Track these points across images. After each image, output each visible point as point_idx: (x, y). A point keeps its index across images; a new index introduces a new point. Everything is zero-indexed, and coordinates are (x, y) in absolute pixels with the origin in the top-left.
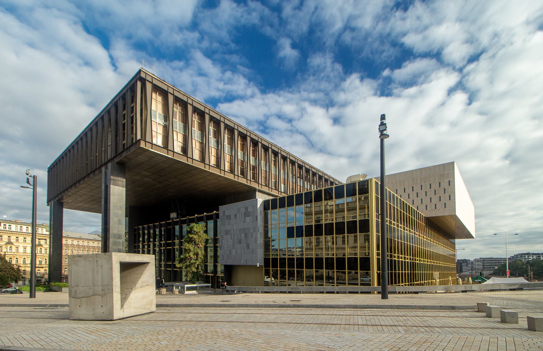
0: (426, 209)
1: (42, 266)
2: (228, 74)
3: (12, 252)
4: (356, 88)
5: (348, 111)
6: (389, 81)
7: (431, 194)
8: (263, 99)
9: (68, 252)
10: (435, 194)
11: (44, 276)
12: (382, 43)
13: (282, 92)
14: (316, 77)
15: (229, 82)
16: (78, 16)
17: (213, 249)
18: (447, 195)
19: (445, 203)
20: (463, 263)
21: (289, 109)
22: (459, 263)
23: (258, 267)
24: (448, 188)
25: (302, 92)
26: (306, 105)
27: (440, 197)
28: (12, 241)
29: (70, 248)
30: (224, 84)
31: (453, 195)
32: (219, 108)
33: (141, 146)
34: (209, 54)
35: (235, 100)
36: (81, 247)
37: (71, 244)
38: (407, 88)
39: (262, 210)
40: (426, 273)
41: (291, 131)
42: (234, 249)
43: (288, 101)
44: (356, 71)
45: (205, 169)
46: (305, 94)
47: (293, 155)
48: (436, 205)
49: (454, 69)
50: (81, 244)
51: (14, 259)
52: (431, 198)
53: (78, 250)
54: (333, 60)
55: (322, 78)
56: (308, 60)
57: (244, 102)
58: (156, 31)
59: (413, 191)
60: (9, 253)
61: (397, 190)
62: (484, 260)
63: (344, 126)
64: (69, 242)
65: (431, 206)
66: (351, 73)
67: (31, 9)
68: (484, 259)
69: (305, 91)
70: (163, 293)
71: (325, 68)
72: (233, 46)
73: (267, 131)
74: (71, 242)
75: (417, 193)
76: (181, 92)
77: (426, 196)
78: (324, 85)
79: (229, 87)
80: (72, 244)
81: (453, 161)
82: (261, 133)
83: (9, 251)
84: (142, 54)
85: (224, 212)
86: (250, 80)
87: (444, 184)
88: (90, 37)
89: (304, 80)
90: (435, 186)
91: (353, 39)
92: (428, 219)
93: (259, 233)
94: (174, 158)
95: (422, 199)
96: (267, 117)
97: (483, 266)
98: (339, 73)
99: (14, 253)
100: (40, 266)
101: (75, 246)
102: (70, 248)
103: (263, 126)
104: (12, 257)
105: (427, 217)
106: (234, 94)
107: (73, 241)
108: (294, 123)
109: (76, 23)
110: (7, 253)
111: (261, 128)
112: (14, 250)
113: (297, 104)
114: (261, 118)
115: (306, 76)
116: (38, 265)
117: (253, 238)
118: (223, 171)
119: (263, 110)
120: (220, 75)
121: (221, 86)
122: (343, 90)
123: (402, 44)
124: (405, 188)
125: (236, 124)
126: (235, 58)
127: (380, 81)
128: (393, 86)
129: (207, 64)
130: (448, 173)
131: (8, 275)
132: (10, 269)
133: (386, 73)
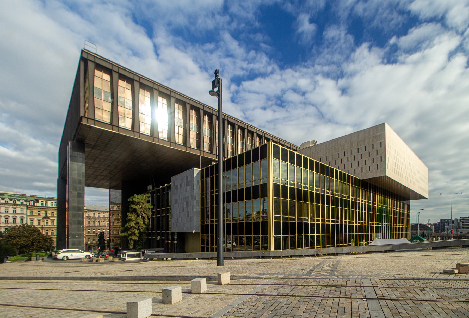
0: (362, 172)
2: (252, 53)
3: (48, 225)
4: (364, 58)
5: (356, 81)
6: (395, 48)
7: (366, 156)
8: (281, 75)
9: (96, 223)
10: (369, 156)
12: (391, 12)
13: (298, 67)
14: (330, 50)
15: (253, 60)
16: (129, 8)
17: (56, 219)
18: (379, 156)
19: (377, 165)
20: (445, 223)
21: (303, 83)
22: (442, 223)
23: (194, 234)
24: (380, 150)
25: (316, 66)
26: (319, 78)
27: (373, 159)
28: (49, 215)
29: (97, 220)
30: (248, 63)
31: (384, 157)
32: (242, 85)
33: (82, 123)
34: (236, 35)
35: (257, 77)
36: (106, 218)
37: (98, 216)
38: (411, 54)
39: (199, 179)
40: (398, 233)
41: (305, 103)
42: (180, 217)
43: (303, 76)
44: (365, 41)
45: (153, 142)
46: (318, 68)
47: (251, 126)
48: (369, 166)
49: (457, 33)
50: (93, 216)
51: (50, 231)
52: (366, 160)
53: (104, 222)
54: (347, 31)
55: (336, 50)
56: (324, 33)
57: (264, 78)
58: (192, 19)
60: (46, 226)
61: (338, 154)
62: (464, 219)
63: (351, 96)
64: (97, 215)
65: (366, 169)
66: (361, 43)
67: (90, 6)
68: (464, 218)
69: (319, 64)
70: (100, 261)
71: (339, 40)
72: (257, 24)
73: (284, 104)
74: (98, 214)
75: (355, 156)
76: (127, 70)
77: (362, 158)
78: (337, 57)
79: (252, 66)
80: (99, 217)
82: (279, 107)
83: (45, 224)
84: (180, 39)
85: (174, 183)
86: (270, 58)
87: (377, 146)
88: (138, 27)
89: (319, 53)
90: (369, 148)
91: (365, 10)
92: (365, 182)
93: (195, 202)
94: (120, 133)
95: (358, 162)
96: (284, 92)
97: (463, 224)
98: (351, 45)
99: (50, 225)
101: (102, 218)
102: (97, 220)
103: (280, 100)
104: (48, 230)
105: (362, 179)
106: (257, 72)
107: (100, 214)
108: (307, 96)
109: (126, 15)
111: (279, 102)
112: (50, 223)
113: (312, 78)
114: (279, 93)
115: (321, 50)
117: (191, 206)
118: (173, 144)
119: (281, 85)
120: (245, 55)
121: (245, 65)
122: (353, 61)
123: (409, 12)
124: (345, 152)
126: (259, 37)
127: (387, 49)
128: (398, 52)
129: (233, 45)
130: (380, 135)
131: (40, 246)
132: (43, 240)
133: (393, 41)
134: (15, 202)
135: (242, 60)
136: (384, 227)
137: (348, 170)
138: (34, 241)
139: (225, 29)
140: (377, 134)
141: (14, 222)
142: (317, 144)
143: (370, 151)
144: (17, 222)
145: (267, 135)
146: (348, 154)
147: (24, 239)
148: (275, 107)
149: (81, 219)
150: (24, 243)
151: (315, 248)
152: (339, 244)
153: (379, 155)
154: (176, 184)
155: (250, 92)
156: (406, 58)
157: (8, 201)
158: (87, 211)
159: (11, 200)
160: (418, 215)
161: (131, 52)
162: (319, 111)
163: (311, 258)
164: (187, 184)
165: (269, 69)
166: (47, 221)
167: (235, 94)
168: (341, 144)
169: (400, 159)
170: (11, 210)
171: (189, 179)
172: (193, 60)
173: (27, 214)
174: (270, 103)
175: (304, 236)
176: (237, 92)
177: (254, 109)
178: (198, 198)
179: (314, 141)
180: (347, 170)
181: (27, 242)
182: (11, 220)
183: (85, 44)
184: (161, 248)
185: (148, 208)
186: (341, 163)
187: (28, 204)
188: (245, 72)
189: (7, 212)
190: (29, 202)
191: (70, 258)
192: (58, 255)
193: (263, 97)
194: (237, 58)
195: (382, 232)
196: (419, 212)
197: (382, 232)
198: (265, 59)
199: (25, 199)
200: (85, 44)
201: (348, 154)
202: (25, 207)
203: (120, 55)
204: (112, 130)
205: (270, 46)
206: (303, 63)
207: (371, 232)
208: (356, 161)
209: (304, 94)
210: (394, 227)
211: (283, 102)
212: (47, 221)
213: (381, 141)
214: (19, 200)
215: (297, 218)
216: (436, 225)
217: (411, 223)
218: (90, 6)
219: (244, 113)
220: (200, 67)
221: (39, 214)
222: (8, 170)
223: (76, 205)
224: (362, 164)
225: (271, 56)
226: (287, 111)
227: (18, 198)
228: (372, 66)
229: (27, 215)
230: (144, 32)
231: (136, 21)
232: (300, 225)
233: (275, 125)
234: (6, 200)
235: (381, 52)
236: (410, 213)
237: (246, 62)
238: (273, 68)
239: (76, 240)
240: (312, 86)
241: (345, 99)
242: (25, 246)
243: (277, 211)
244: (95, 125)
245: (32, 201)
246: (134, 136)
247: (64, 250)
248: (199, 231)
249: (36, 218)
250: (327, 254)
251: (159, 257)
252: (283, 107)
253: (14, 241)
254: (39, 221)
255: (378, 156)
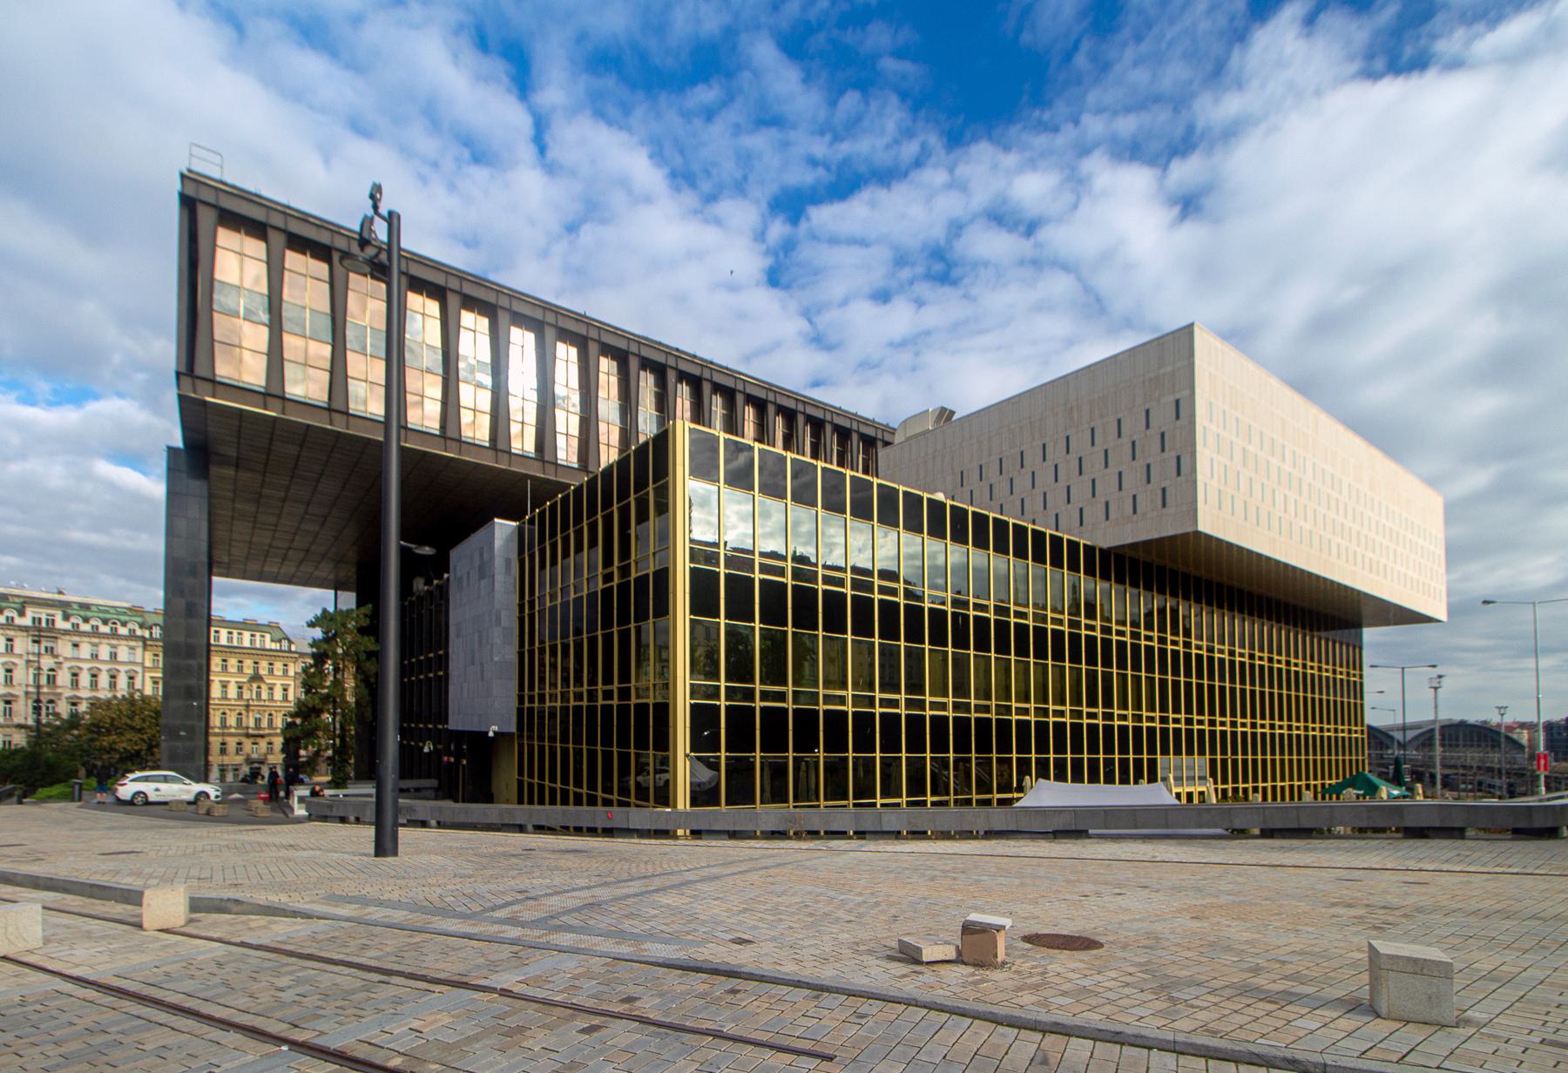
0: (1107, 518)
1: (261, 732)
2: (850, 101)
8: (951, 170)
10: (1134, 458)
11: (266, 759)
13: (1014, 130)
14: (1144, 47)
15: (853, 127)
18: (1170, 455)
25: (1086, 119)
27: (1148, 466)
30: (837, 138)
32: (808, 219)
34: (794, 46)
43: (1031, 164)
52: (1120, 474)
59: (1068, 452)
61: (1022, 453)
65: (1094, 512)
67: (357, 20)
69: (1099, 111)
73: (955, 273)
75: (1080, 459)
81: (1189, 322)
84: (610, 82)
86: (915, 109)
89: (1103, 67)
90: (1133, 426)
96: (956, 228)
100: (256, 732)
106: (862, 169)
108: (1043, 234)
110: (251, 703)
111: (938, 267)
114: (938, 233)
116: (253, 729)
119: (951, 205)
121: (820, 148)
122: (1239, 84)
125: (506, 291)
128: (1439, 18)
134: (116, 629)
135: (813, 133)
136: (1314, 737)
137: (1058, 511)
138: (154, 743)
139: (758, 27)
140: (1162, 371)
141: (113, 686)
142: (954, 418)
143: (1135, 437)
144: (118, 687)
145: (785, 398)
146: (1056, 453)
147: (128, 736)
148: (923, 289)
149: (193, 682)
150: (129, 748)
151: (874, 805)
152: (991, 792)
153: (1170, 450)
154: (458, 575)
155: (834, 241)
156: (1468, 43)
157: (78, 625)
158: (297, 655)
159: (105, 622)
160: (1436, 688)
161: (466, 154)
162: (1087, 289)
163: (855, 843)
164: (482, 575)
165: (910, 149)
166: (259, 687)
167: (781, 255)
168: (1030, 417)
169: (1274, 461)
170: (104, 652)
171: (486, 556)
172: (651, 157)
173: (142, 664)
174: (905, 274)
175: (931, 758)
176: (788, 246)
177: (844, 303)
178: (510, 619)
179: (943, 410)
180: (1054, 513)
181: (136, 744)
182: (104, 680)
183: (191, 155)
184: (428, 780)
185: (365, 652)
186: (1033, 487)
187: (147, 634)
188: (821, 171)
189: (95, 657)
190: (150, 628)
191: (153, 797)
192: (120, 788)
193: (883, 254)
194: (794, 127)
195: (1213, 752)
196: (1440, 677)
197: (1213, 752)
198: (892, 115)
199: (139, 620)
200: (191, 155)
201: (1056, 453)
202: (141, 644)
203: (435, 165)
204: (266, 409)
205: (914, 61)
206: (1037, 113)
207: (1152, 750)
208: (1086, 478)
209: (1031, 228)
210: (1336, 738)
211: (950, 265)
212: (259, 687)
213: (1178, 396)
214: (124, 624)
215: (853, 695)
216: (1555, 731)
217: (1367, 721)
218: (357, 20)
219: (810, 321)
220: (673, 175)
221: (240, 669)
222: (144, 536)
223: (181, 639)
224: (1107, 487)
225: (918, 102)
226: (966, 297)
227: (123, 618)
228: (1318, 93)
229: (144, 668)
230: (506, 80)
231: (482, 43)
232: (806, 719)
233: (917, 354)
234: (93, 622)
235: (1359, 31)
236: (1361, 677)
237: (828, 137)
238: (924, 146)
239: (180, 744)
240: (1068, 198)
241: (1192, 234)
242: (132, 755)
243: (704, 664)
244: (214, 397)
245: (156, 625)
246: (331, 424)
247: (138, 774)
248: (513, 729)
249: (233, 680)
250: (826, 833)
251: (331, 810)
252: (954, 283)
253: (106, 741)
254: (240, 688)
255: (1165, 455)
